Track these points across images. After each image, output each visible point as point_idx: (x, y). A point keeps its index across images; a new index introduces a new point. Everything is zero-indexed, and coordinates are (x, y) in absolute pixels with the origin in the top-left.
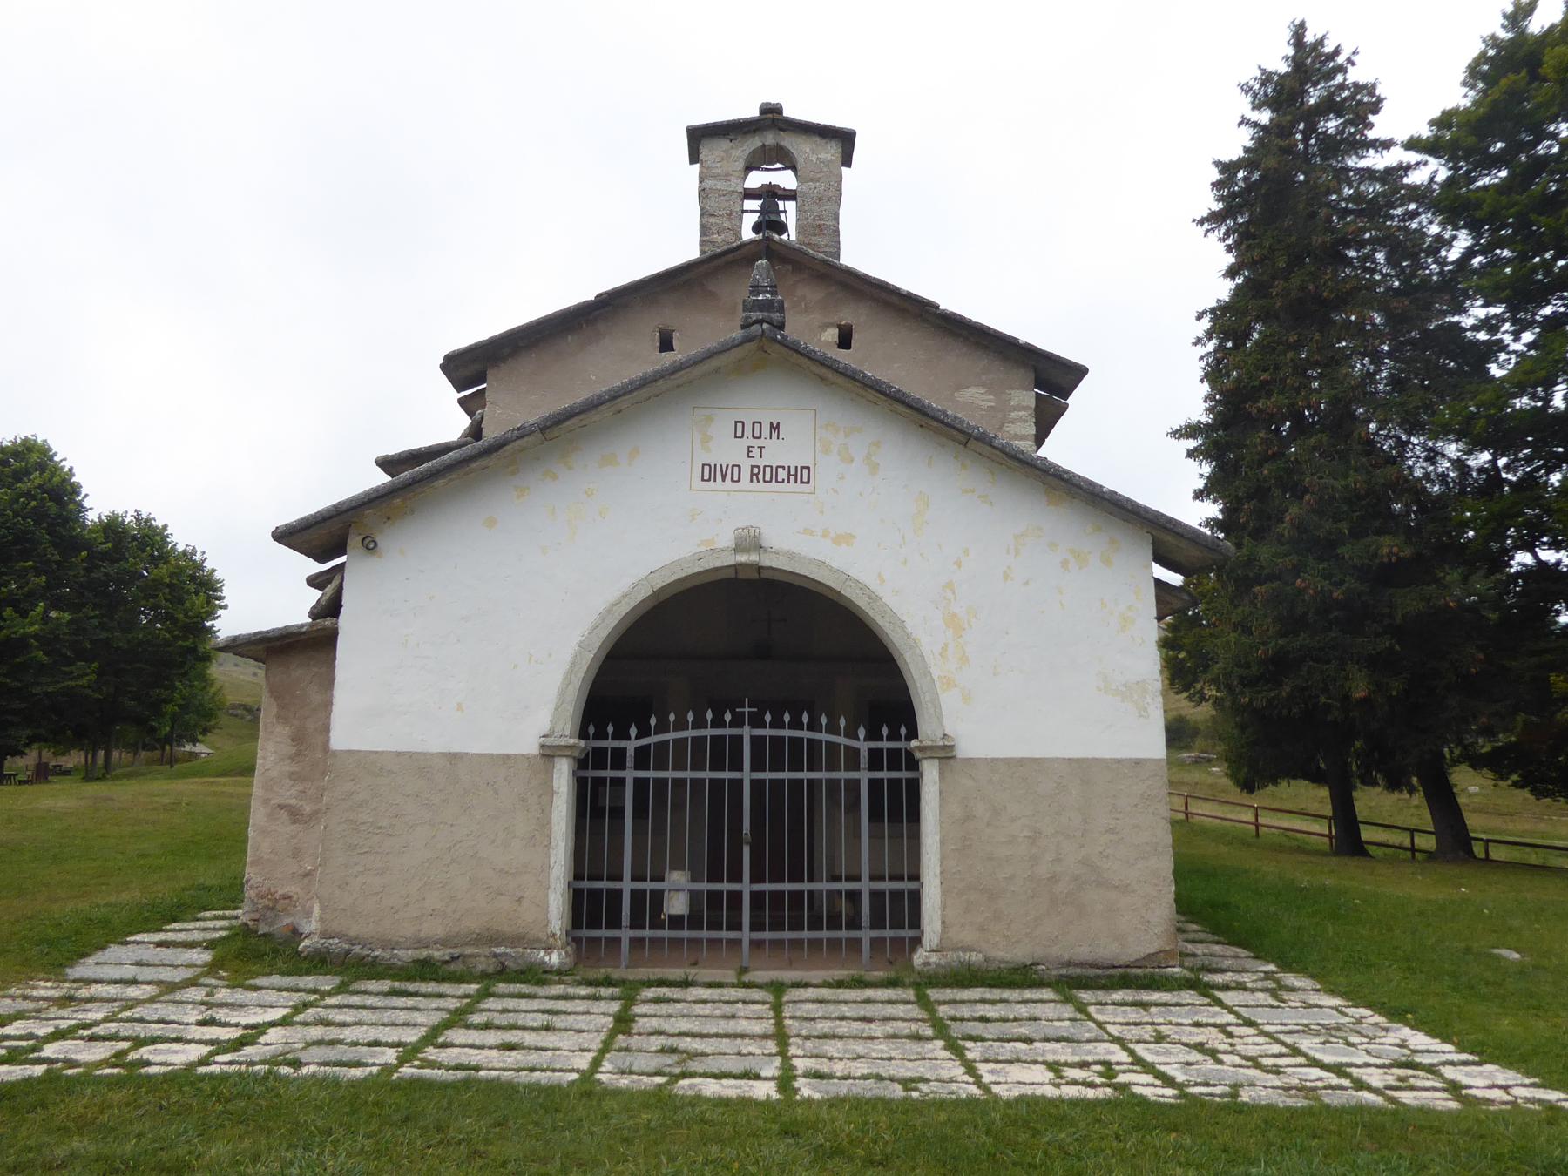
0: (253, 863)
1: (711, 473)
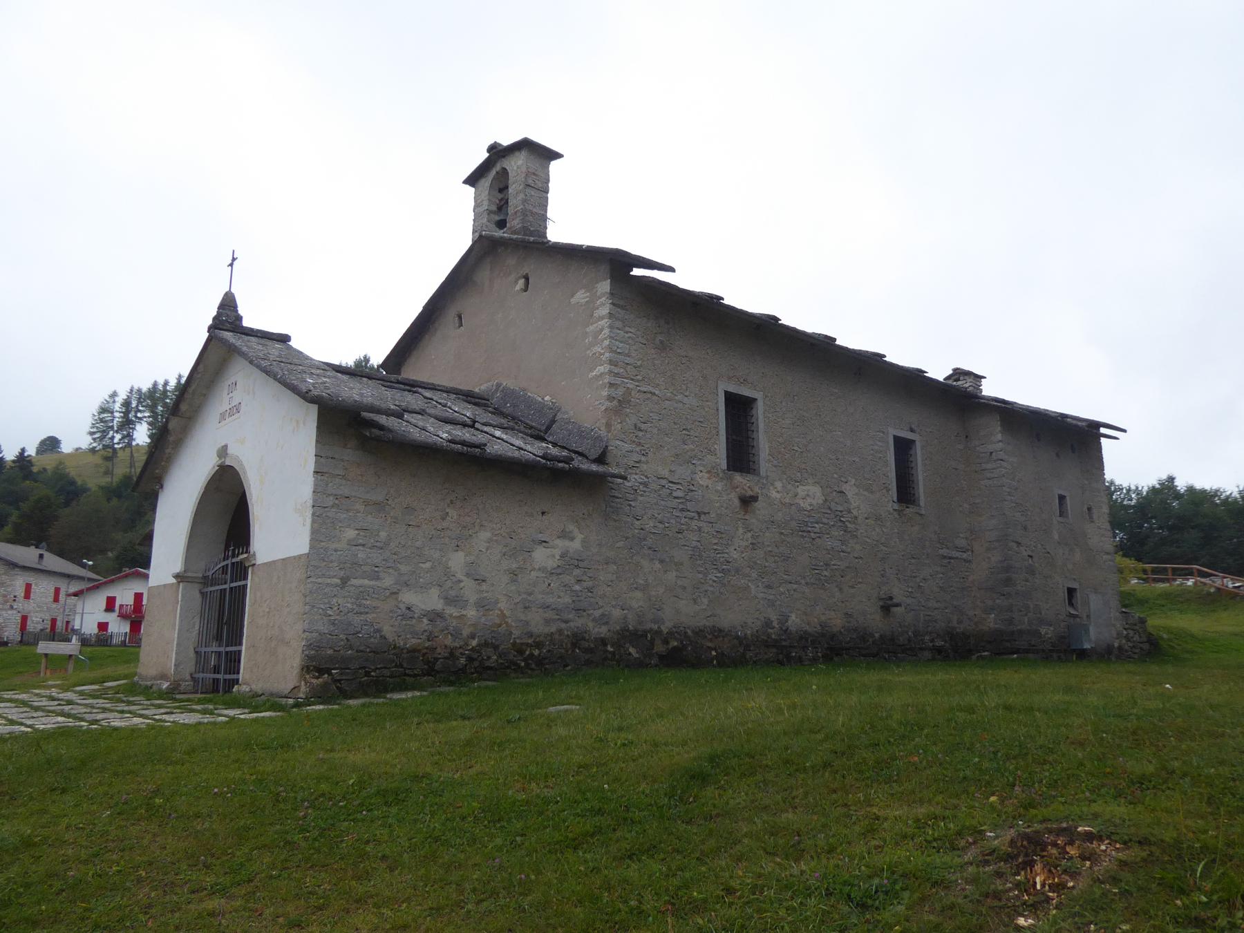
1: (223, 417)
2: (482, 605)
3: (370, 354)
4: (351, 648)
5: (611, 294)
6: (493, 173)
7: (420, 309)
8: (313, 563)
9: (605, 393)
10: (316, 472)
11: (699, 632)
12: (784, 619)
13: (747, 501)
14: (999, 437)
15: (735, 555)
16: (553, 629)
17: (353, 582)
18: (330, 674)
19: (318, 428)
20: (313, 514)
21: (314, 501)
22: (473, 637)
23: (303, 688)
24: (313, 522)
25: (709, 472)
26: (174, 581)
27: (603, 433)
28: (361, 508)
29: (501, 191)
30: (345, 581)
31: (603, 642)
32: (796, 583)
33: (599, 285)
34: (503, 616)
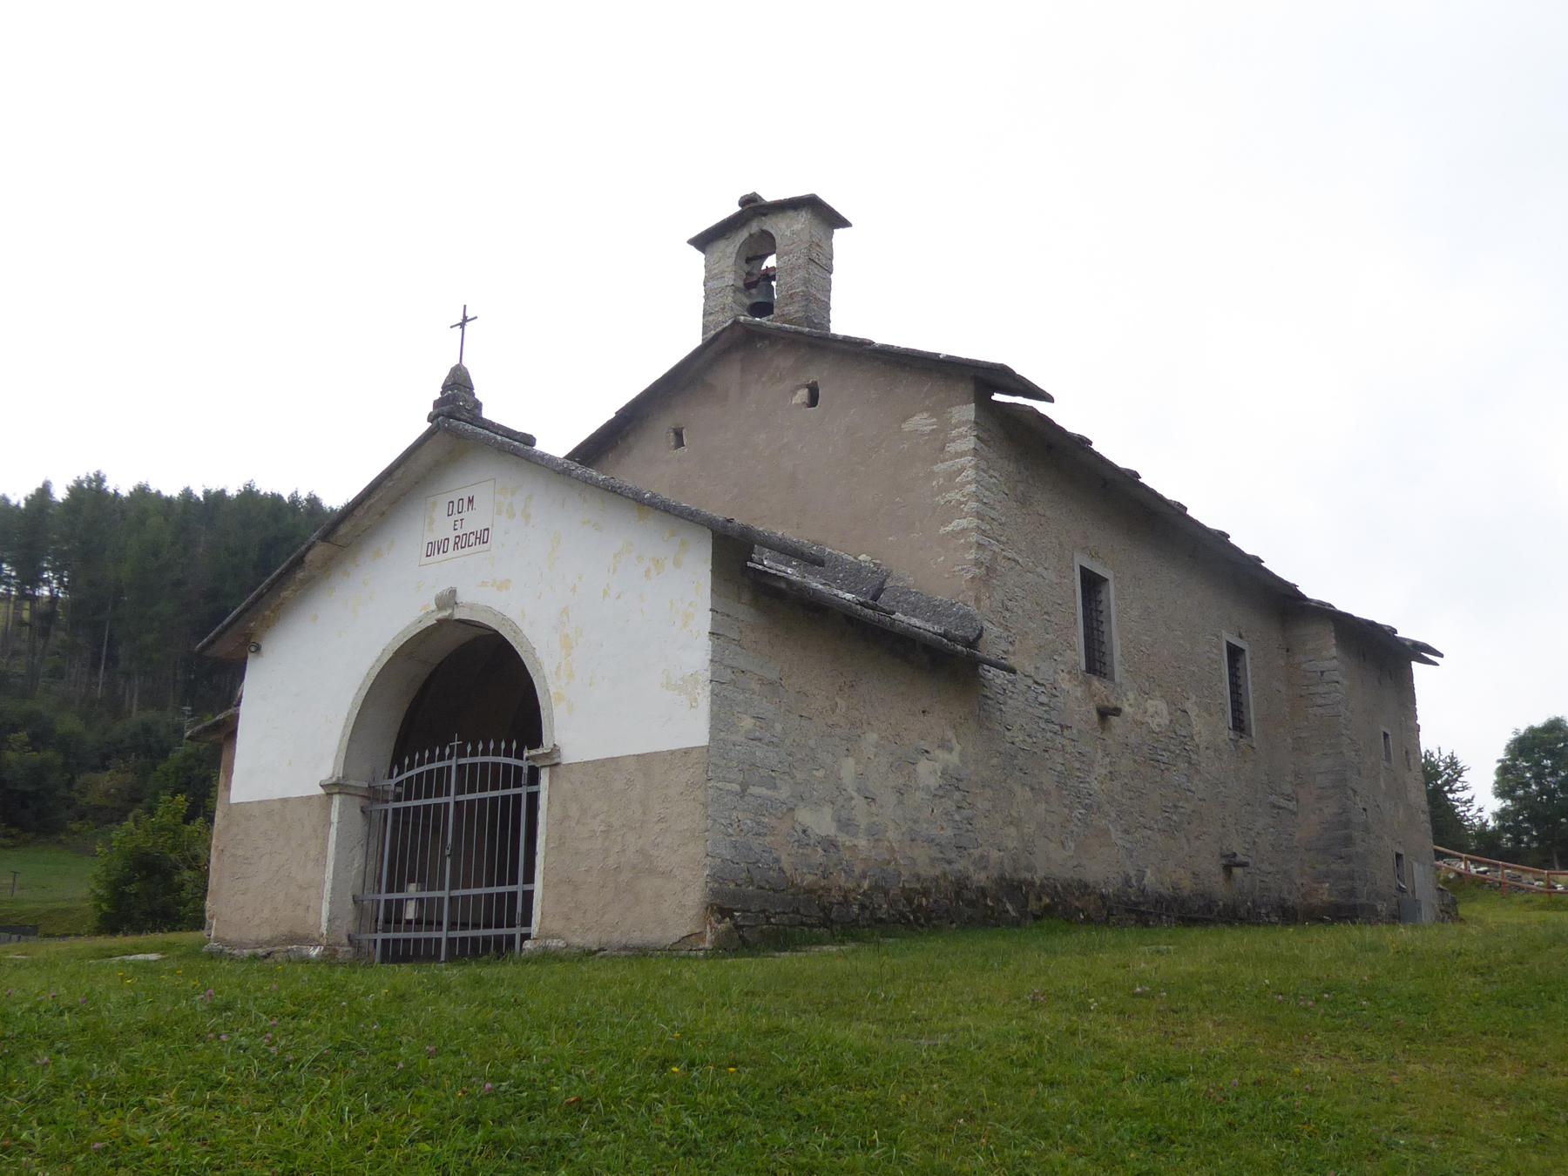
0: (479, 982)
1: (437, 548)
2: (875, 834)
3: (104, 472)
4: (752, 882)
5: (976, 423)
6: (744, 234)
7: (611, 415)
8: (713, 760)
9: (971, 555)
10: (712, 633)
11: (1067, 887)
12: (1141, 875)
13: (1105, 713)
14: (1334, 651)
15: (1096, 785)
16: (938, 872)
17: (753, 790)
18: (732, 917)
19: (715, 572)
20: (712, 692)
21: (713, 673)
22: (864, 876)
23: (709, 936)
24: (713, 703)
25: (1069, 673)
26: (321, 791)
27: (972, 608)
28: (755, 686)
29: (748, 260)
30: (743, 792)
31: (983, 892)
32: (1151, 829)
33: (955, 410)
34: (892, 850)
